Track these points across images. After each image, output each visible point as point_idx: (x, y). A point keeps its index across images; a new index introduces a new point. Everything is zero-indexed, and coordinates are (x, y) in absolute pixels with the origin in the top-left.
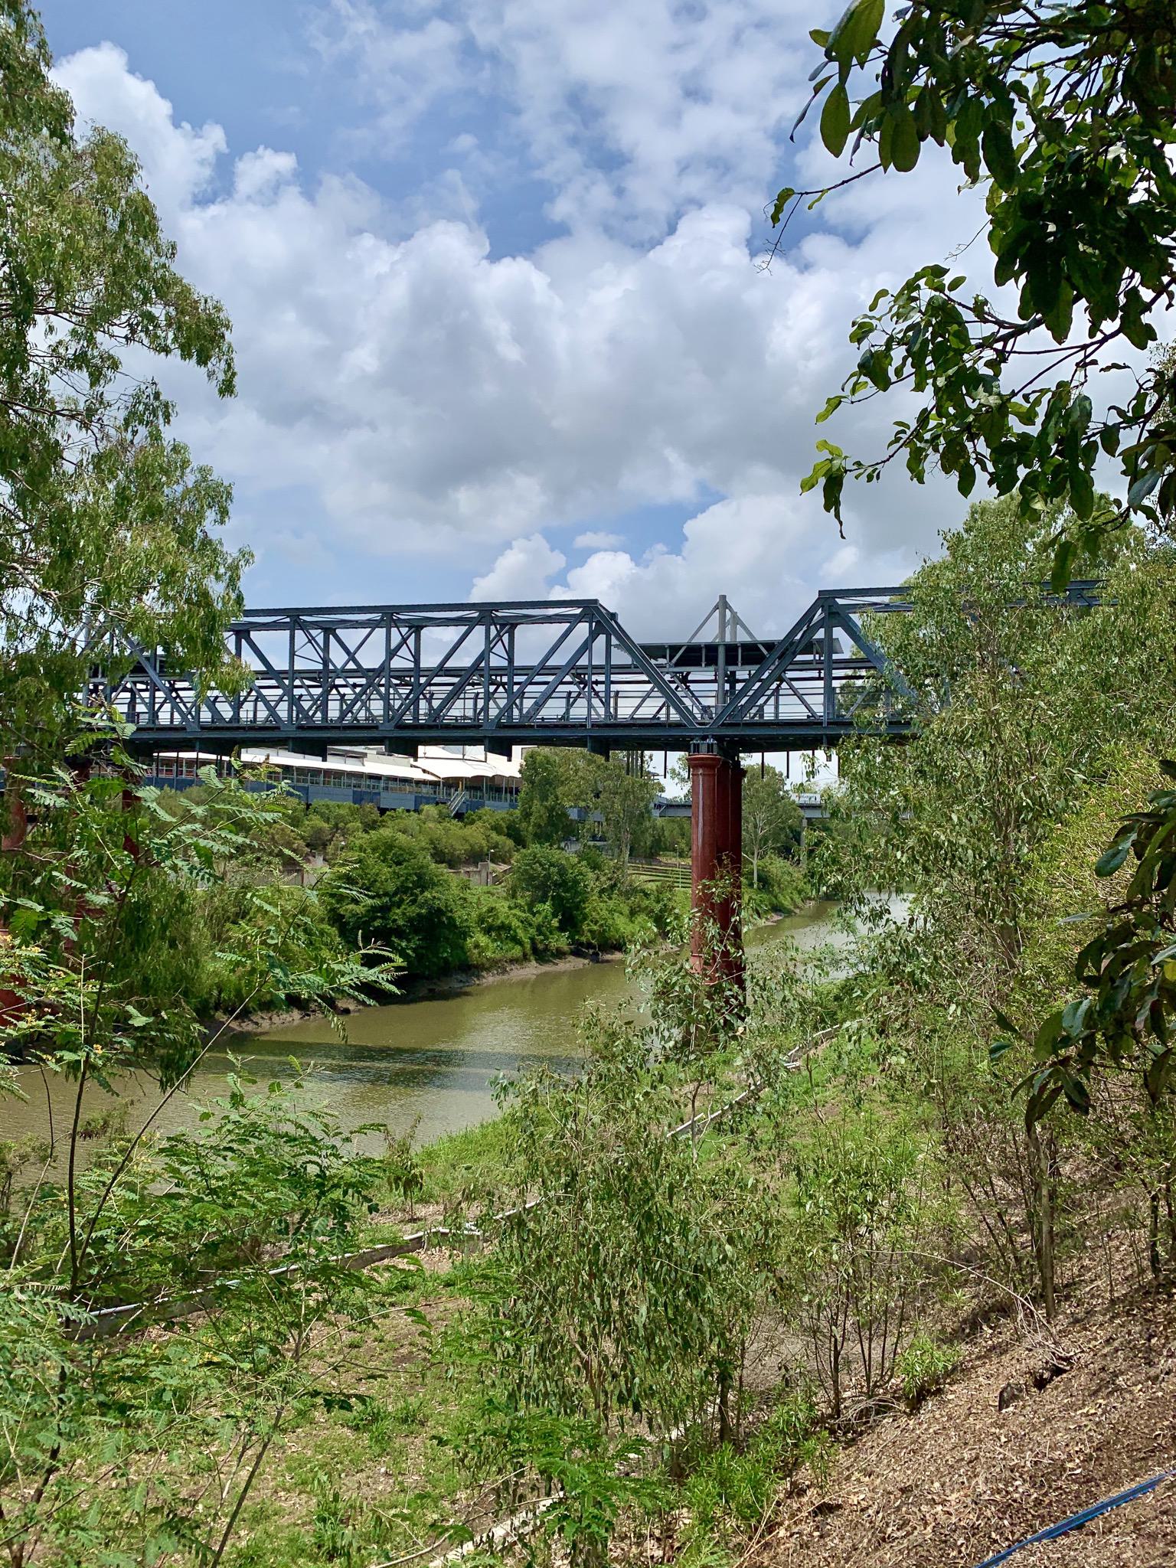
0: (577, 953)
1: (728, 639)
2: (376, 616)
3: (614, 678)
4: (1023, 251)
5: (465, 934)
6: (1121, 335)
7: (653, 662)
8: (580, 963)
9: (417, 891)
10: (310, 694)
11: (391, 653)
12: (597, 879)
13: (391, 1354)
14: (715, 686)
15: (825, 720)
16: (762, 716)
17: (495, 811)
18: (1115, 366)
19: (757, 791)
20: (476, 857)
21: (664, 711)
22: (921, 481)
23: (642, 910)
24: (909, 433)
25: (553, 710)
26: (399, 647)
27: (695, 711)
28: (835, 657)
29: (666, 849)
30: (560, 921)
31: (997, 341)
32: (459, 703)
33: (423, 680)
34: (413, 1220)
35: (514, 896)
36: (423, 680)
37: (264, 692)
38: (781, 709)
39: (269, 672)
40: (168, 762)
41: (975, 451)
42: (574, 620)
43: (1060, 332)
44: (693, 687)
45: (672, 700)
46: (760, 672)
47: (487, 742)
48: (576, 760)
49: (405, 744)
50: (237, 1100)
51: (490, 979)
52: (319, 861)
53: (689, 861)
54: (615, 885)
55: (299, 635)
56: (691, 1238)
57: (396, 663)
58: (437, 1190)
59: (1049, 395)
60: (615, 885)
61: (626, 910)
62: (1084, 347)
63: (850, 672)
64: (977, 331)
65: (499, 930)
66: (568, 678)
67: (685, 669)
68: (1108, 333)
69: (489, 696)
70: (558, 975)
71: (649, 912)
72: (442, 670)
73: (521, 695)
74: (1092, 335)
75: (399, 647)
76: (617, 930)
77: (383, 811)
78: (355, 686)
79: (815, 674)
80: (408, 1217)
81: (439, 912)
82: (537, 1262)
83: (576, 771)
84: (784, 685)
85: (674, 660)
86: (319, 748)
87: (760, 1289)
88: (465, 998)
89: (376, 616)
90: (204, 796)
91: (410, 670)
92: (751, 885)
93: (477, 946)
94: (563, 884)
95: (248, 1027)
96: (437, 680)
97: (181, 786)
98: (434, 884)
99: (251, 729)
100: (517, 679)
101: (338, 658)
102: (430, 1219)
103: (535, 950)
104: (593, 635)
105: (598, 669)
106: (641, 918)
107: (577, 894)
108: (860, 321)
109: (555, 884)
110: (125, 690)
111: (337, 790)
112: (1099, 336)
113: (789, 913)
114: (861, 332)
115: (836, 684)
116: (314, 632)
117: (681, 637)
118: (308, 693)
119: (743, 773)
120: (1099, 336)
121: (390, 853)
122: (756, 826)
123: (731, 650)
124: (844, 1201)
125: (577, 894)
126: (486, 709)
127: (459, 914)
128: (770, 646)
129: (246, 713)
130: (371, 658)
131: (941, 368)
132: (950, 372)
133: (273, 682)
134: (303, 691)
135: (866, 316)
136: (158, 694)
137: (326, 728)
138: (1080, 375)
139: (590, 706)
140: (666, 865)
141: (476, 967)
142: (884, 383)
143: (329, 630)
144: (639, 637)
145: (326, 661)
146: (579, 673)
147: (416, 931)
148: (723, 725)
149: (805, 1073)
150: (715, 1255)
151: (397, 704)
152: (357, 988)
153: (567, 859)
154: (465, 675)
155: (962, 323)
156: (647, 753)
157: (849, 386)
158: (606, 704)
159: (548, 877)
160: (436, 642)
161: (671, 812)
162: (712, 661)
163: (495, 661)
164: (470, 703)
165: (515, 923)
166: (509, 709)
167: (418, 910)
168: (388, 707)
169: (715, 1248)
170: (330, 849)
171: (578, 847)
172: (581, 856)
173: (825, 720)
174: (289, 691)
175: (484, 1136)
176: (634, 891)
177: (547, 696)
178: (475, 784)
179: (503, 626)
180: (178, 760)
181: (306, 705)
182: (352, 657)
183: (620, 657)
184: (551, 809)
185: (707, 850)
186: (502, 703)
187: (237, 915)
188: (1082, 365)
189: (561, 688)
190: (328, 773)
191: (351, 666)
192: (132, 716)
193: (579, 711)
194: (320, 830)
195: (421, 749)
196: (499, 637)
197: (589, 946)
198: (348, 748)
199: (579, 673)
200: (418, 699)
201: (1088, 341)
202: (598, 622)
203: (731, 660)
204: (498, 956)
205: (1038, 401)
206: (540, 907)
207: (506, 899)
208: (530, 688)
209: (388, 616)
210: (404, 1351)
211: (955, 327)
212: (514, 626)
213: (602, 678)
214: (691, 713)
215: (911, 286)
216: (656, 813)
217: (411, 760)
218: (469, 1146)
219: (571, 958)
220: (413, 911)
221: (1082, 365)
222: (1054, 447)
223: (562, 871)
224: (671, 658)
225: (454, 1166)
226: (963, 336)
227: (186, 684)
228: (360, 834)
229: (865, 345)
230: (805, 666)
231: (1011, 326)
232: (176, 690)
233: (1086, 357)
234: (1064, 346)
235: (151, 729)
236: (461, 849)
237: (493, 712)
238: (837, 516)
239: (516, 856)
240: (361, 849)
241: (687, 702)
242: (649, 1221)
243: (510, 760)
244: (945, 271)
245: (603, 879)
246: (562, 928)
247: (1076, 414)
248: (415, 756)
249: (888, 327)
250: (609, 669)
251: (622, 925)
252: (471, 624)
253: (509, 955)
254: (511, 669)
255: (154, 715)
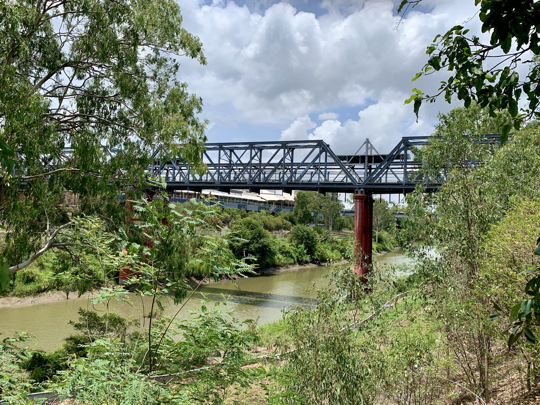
0: (313, 262)
1: (369, 154)
2: (247, 146)
3: (328, 167)
4: (493, 21)
5: (274, 254)
6: (530, 50)
7: (342, 162)
8: (314, 266)
9: (258, 239)
10: (225, 172)
11: (252, 158)
12: (320, 237)
13: (249, 398)
14: (364, 170)
15: (404, 183)
16: (381, 181)
17: (286, 212)
18: (528, 61)
19: (378, 207)
20: (278, 228)
21: (345, 179)
22: (449, 102)
23: (336, 248)
24: (446, 85)
25: (306, 178)
26: (254, 156)
27: (357, 179)
28: (408, 160)
29: (345, 227)
30: (307, 251)
31: (481, 52)
32: (274, 175)
33: (262, 167)
34: (257, 352)
35: (291, 242)
36: (262, 167)
37: (210, 171)
38: (388, 179)
39: (212, 164)
40: (178, 193)
41: (471, 92)
42: (314, 147)
43: (506, 49)
44: (356, 170)
45: (348, 175)
46: (380, 166)
47: (283, 189)
48: (314, 196)
49: (256, 189)
50: (204, 308)
51: (282, 270)
52: (226, 228)
53: (353, 232)
54: (326, 239)
55: (222, 152)
56: (356, 366)
57: (254, 162)
58: (264, 342)
59: (501, 72)
60: (326, 239)
61: (330, 248)
62: (516, 54)
63: (413, 166)
64: (474, 49)
65: (286, 253)
66: (312, 167)
67: (353, 164)
68: (525, 49)
69: (284, 173)
70: (306, 270)
71: (338, 249)
72: (269, 164)
73: (296, 173)
74: (518, 49)
75: (254, 156)
76: (327, 255)
77: (248, 211)
78: (240, 169)
79: (400, 166)
80: (255, 351)
81: (266, 246)
82: (302, 371)
83: (314, 199)
84: (389, 170)
85: (349, 161)
86: (227, 190)
87: (378, 386)
88: (274, 276)
89: (247, 146)
90: (190, 205)
91: (258, 164)
92: (375, 241)
93: (278, 258)
94: (308, 238)
95: (202, 282)
96: (267, 167)
97: (182, 201)
98: (264, 237)
99: (206, 183)
100: (294, 167)
101: (234, 159)
102: (262, 352)
103: (298, 261)
104: (321, 152)
105: (322, 164)
106: (336, 251)
107: (313, 242)
108: (429, 46)
109: (305, 238)
110: (165, 169)
111: (233, 204)
112: (521, 50)
113: (389, 251)
114: (431, 50)
115: (408, 170)
116: (227, 151)
117: (352, 153)
118: (224, 172)
119: (374, 201)
120: (521, 50)
121: (249, 225)
122: (377, 220)
123: (370, 157)
124: (409, 355)
125: (313, 242)
126: (283, 177)
127: (273, 247)
128: (384, 156)
129: (204, 178)
130: (245, 160)
131: (460, 62)
132: (464, 63)
133: (213, 168)
134: (222, 171)
135: (432, 44)
136: (176, 171)
137: (230, 183)
138: (514, 65)
139: (319, 177)
140: (345, 233)
141: (278, 265)
142: (437, 68)
143: (232, 150)
144: (337, 153)
145: (230, 161)
146: (316, 166)
147: (258, 252)
148: (367, 184)
149: (394, 308)
150: (365, 372)
151: (253, 175)
152: (242, 273)
153: (310, 229)
154: (277, 166)
155: (468, 46)
156: (339, 193)
157: (424, 69)
158: (325, 176)
159: (303, 236)
161: (347, 214)
162: (363, 161)
163: (287, 161)
164: (278, 175)
165: (292, 251)
166: (291, 177)
167: (259, 245)
168: (250, 176)
169: (365, 370)
170: (230, 224)
171: (314, 225)
172: (315, 229)
173: (404, 183)
174: (218, 171)
175: (281, 324)
176: (333, 242)
177: (305, 173)
178: (279, 203)
179: (290, 149)
180: (182, 193)
181: (224, 175)
182: (239, 159)
183: (330, 160)
184: (304, 212)
185: (360, 228)
186: (289, 175)
187: (199, 245)
188: (515, 61)
189: (309, 170)
190: (230, 198)
191: (239, 162)
192: (167, 178)
193: (315, 179)
194: (227, 217)
195: (261, 190)
196: (288, 152)
197: (317, 260)
198: (236, 190)
199: (316, 166)
200: (260, 174)
201: (517, 52)
202: (323, 148)
203: (370, 161)
204: (285, 262)
205: (497, 74)
206: (300, 246)
207: (288, 243)
208: (298, 170)
209: (251, 146)
210: (253, 397)
211: (466, 48)
212: (293, 149)
213: (324, 167)
214: (355, 180)
215: (450, 33)
216: (341, 215)
217: (258, 194)
218: (275, 328)
219: (311, 264)
220: (257, 245)
221: (515, 61)
222: (503, 90)
223: (308, 234)
224: (348, 161)
225: (270, 334)
226: (469, 51)
227: (185, 168)
228: (240, 219)
229: (432, 55)
230: (397, 164)
231: (486, 47)
232: (182, 170)
233: (516, 58)
234: (507, 54)
235: (173, 183)
236: (273, 225)
237: (286, 179)
238: (417, 114)
239: (292, 228)
240: (240, 224)
241: (354, 176)
242: (341, 359)
243: (291, 195)
244: (462, 28)
245: (322, 237)
246: (308, 254)
247: (513, 79)
248: (259, 193)
249: (440, 47)
250: (326, 164)
251: (329, 253)
252: (279, 148)
253: (289, 262)
254: (292, 164)
255: (174, 178)
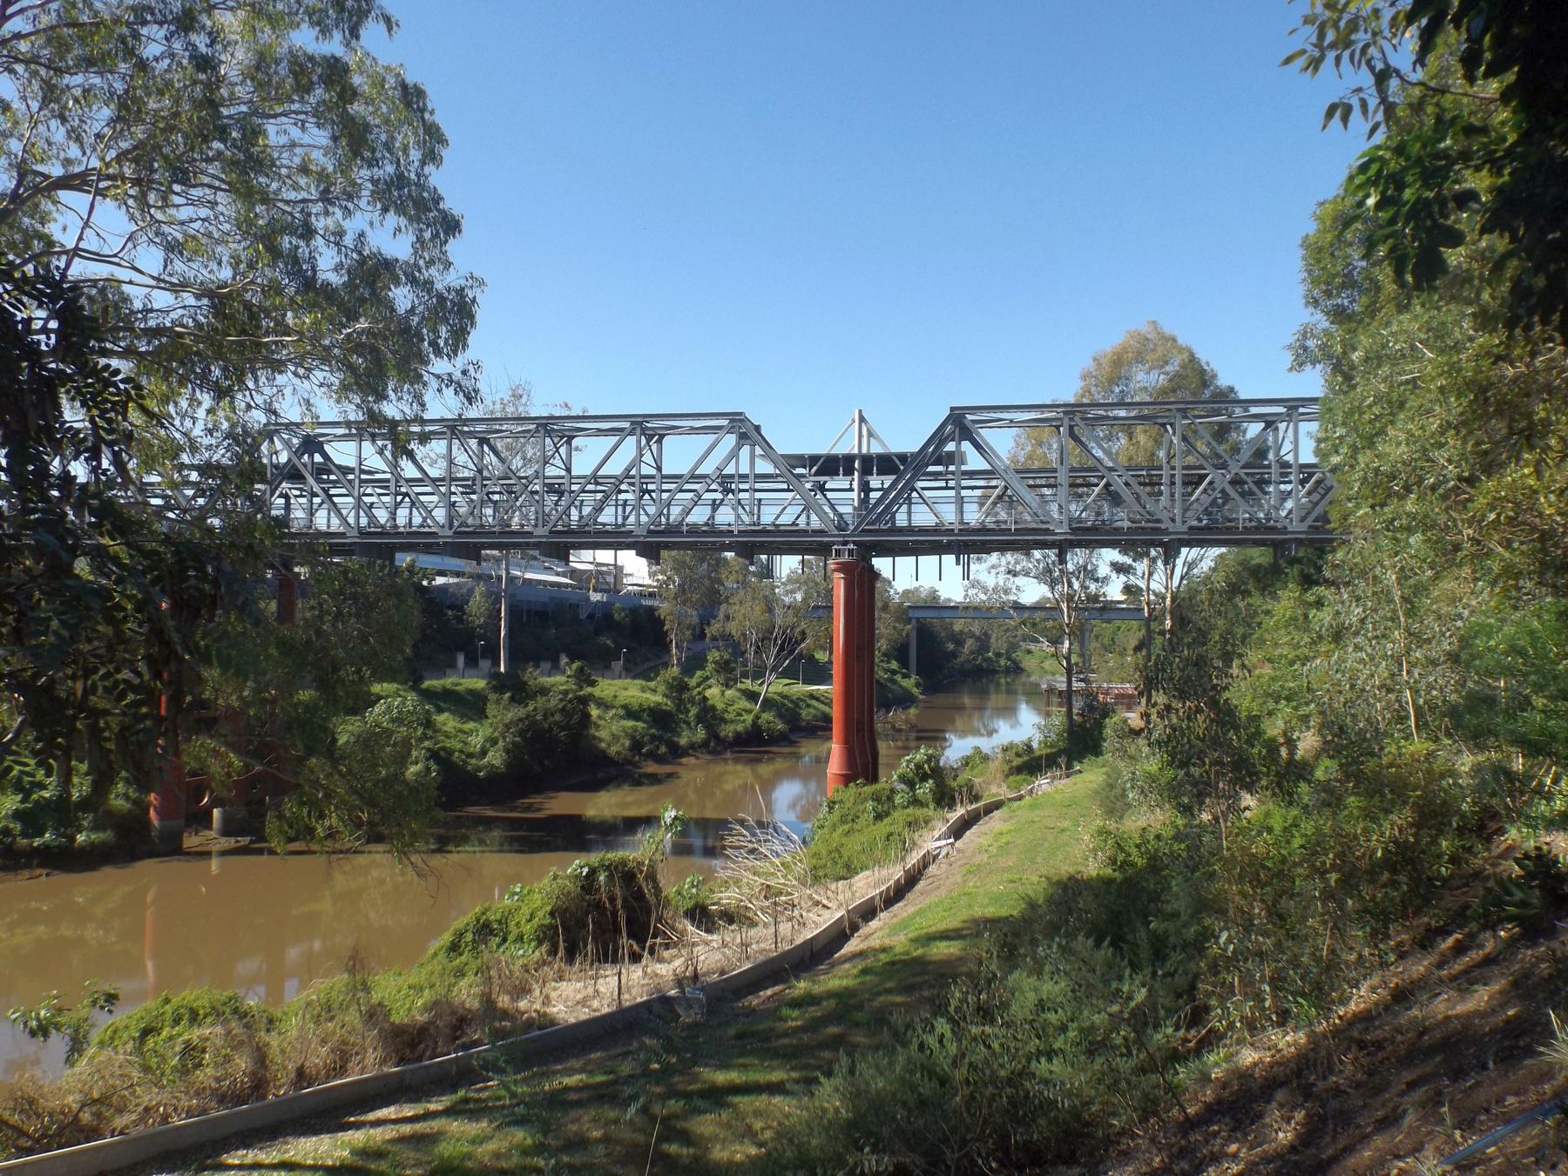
44: (829, 495)
67: (822, 479)
160: (679, 454)
203: (866, 471)
